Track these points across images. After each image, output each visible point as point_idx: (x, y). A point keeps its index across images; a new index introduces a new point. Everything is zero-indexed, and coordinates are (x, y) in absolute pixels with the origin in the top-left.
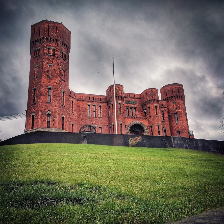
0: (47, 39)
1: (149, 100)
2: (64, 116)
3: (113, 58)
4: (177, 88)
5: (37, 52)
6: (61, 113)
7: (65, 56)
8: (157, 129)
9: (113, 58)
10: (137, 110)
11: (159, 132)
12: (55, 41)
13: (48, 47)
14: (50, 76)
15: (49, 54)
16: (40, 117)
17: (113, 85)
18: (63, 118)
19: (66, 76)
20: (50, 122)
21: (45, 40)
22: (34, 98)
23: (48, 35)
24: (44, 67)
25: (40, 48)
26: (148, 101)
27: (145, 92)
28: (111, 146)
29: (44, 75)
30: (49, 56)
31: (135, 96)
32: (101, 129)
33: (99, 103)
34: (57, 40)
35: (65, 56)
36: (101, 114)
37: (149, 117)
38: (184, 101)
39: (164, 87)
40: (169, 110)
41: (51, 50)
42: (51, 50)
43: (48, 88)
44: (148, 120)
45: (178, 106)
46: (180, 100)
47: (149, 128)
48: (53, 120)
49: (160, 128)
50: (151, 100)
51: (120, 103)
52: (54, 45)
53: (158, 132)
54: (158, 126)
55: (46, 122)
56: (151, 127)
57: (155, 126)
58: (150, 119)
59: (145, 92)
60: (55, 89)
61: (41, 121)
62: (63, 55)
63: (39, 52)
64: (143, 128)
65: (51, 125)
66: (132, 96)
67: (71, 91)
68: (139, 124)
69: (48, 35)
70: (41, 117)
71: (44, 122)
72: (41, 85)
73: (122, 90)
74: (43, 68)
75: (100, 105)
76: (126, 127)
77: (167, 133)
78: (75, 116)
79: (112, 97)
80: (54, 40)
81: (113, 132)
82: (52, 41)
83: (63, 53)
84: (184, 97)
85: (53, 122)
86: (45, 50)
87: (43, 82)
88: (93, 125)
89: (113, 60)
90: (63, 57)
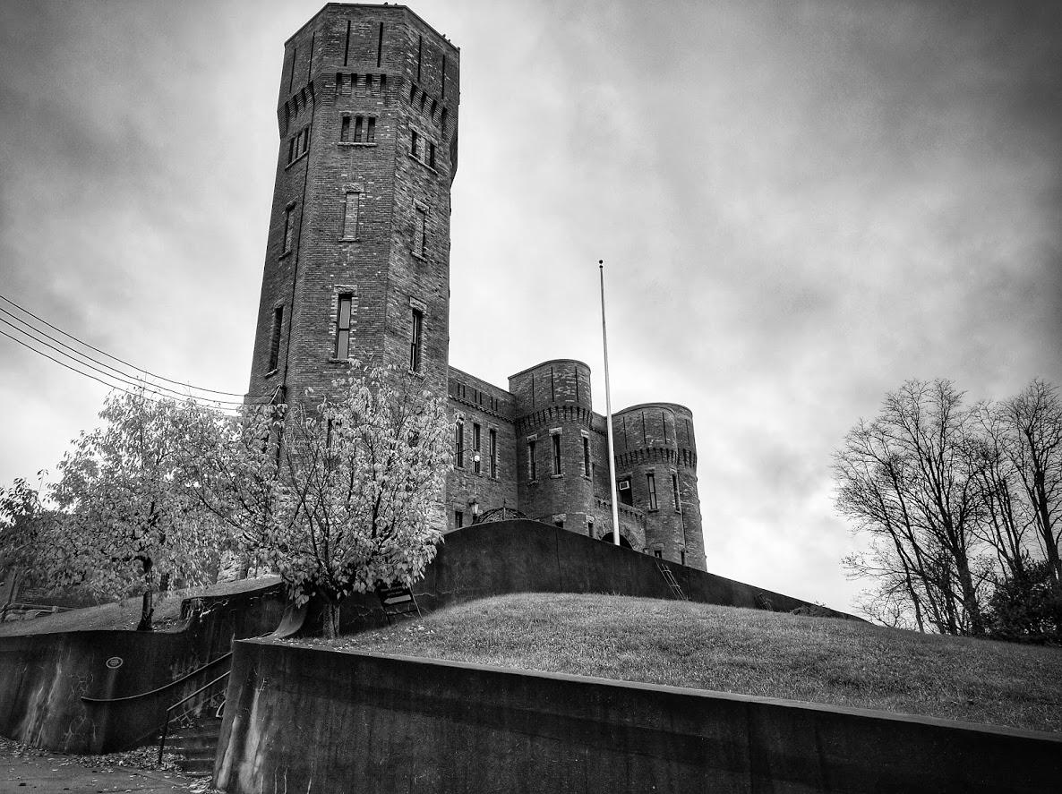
0: (414, 90)
1: (654, 449)
3: (601, 262)
4: (684, 424)
9: (601, 262)
12: (438, 113)
21: (406, 92)
25: (378, 114)
26: (648, 450)
27: (635, 416)
28: (955, 727)
29: (398, 240)
30: (415, 165)
33: (491, 418)
37: (650, 512)
38: (693, 465)
43: (410, 307)
44: (645, 524)
45: (687, 488)
50: (661, 449)
52: (431, 127)
57: (674, 551)
59: (635, 416)
60: (435, 318)
72: (388, 285)
74: (396, 208)
79: (557, 408)
80: (435, 104)
82: (428, 106)
84: (695, 455)
87: (394, 273)
89: (601, 267)
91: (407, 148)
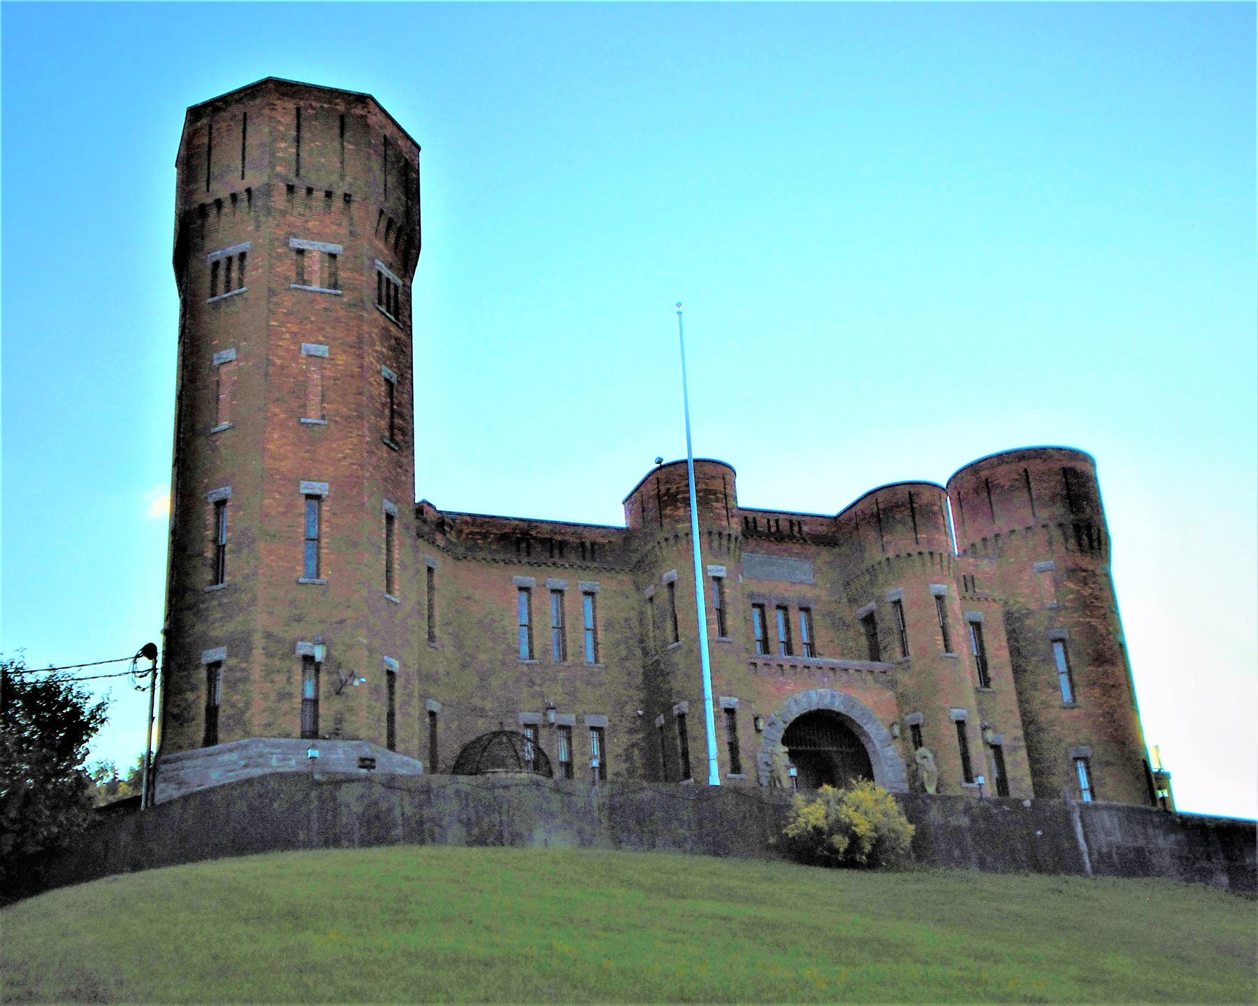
0: (291, 189)
2: (396, 665)
3: (679, 305)
5: (228, 269)
6: (377, 643)
7: (392, 293)
8: (955, 741)
10: (816, 617)
11: (966, 758)
12: (338, 203)
13: (295, 243)
14: (315, 421)
15: (304, 282)
16: (256, 673)
17: (686, 462)
18: (391, 674)
19: (401, 416)
20: (315, 702)
21: (279, 200)
22: (220, 549)
23: (298, 170)
24: (278, 362)
31: (805, 529)
32: (569, 739)
34: (347, 198)
35: (392, 293)
36: (596, 644)
39: (974, 468)
40: (1009, 617)
41: (315, 264)
42: (315, 264)
46: (1082, 551)
47: (902, 731)
48: (338, 693)
49: (969, 733)
51: (718, 574)
53: (959, 762)
54: (961, 724)
55: (297, 702)
56: (916, 728)
58: (901, 676)
61: (266, 696)
62: (384, 289)
63: (242, 268)
64: (864, 733)
65: (321, 725)
66: (784, 525)
67: (424, 502)
68: (838, 707)
69: (298, 170)
70: (268, 673)
71: (285, 706)
73: (727, 495)
75: (587, 585)
76: (758, 731)
77: (1008, 768)
78: (447, 659)
81: (680, 762)
83: (380, 274)
85: (338, 704)
86: (280, 258)
88: (552, 717)
89: (679, 313)
90: (384, 299)
91: (287, 279)
